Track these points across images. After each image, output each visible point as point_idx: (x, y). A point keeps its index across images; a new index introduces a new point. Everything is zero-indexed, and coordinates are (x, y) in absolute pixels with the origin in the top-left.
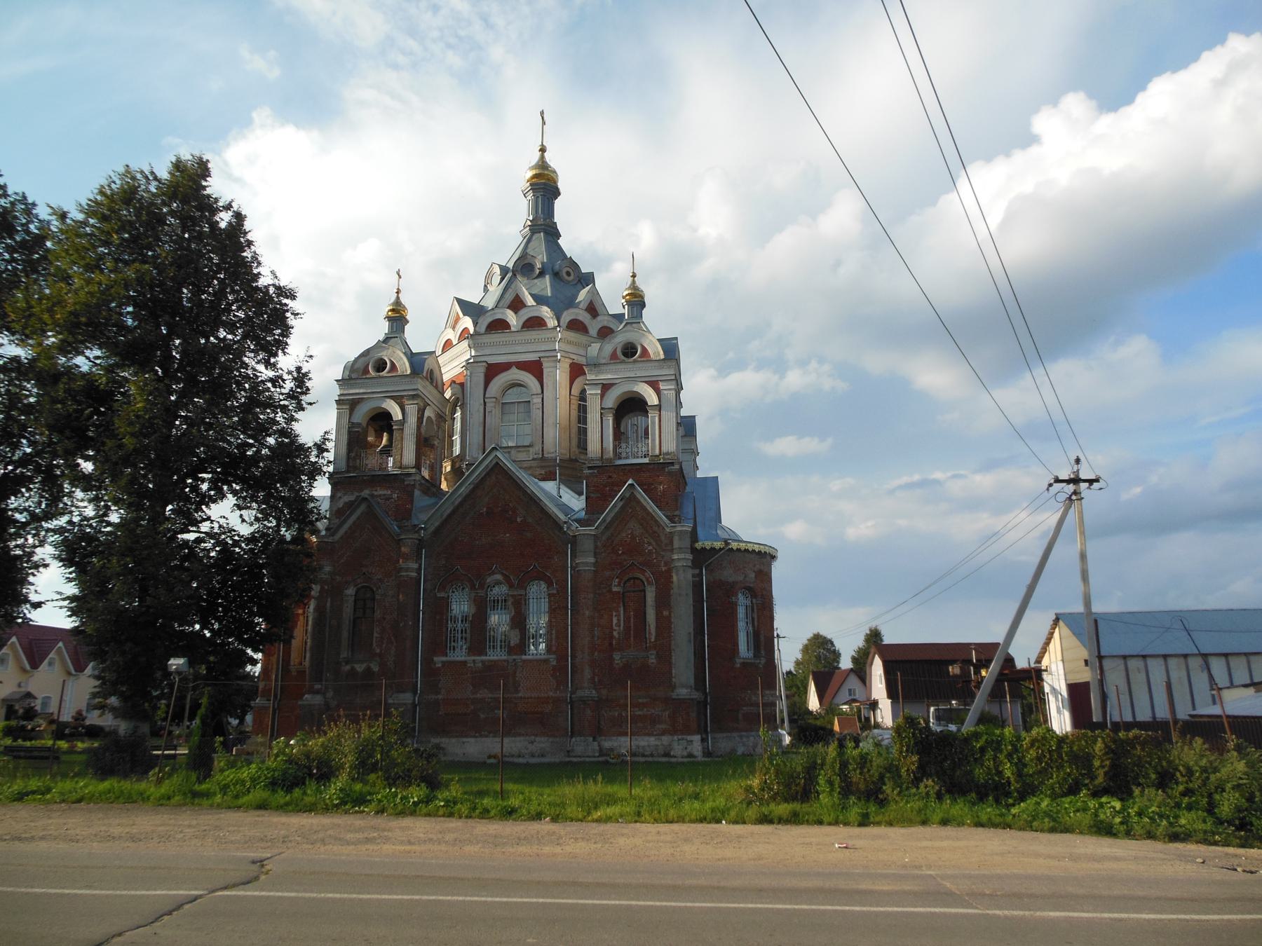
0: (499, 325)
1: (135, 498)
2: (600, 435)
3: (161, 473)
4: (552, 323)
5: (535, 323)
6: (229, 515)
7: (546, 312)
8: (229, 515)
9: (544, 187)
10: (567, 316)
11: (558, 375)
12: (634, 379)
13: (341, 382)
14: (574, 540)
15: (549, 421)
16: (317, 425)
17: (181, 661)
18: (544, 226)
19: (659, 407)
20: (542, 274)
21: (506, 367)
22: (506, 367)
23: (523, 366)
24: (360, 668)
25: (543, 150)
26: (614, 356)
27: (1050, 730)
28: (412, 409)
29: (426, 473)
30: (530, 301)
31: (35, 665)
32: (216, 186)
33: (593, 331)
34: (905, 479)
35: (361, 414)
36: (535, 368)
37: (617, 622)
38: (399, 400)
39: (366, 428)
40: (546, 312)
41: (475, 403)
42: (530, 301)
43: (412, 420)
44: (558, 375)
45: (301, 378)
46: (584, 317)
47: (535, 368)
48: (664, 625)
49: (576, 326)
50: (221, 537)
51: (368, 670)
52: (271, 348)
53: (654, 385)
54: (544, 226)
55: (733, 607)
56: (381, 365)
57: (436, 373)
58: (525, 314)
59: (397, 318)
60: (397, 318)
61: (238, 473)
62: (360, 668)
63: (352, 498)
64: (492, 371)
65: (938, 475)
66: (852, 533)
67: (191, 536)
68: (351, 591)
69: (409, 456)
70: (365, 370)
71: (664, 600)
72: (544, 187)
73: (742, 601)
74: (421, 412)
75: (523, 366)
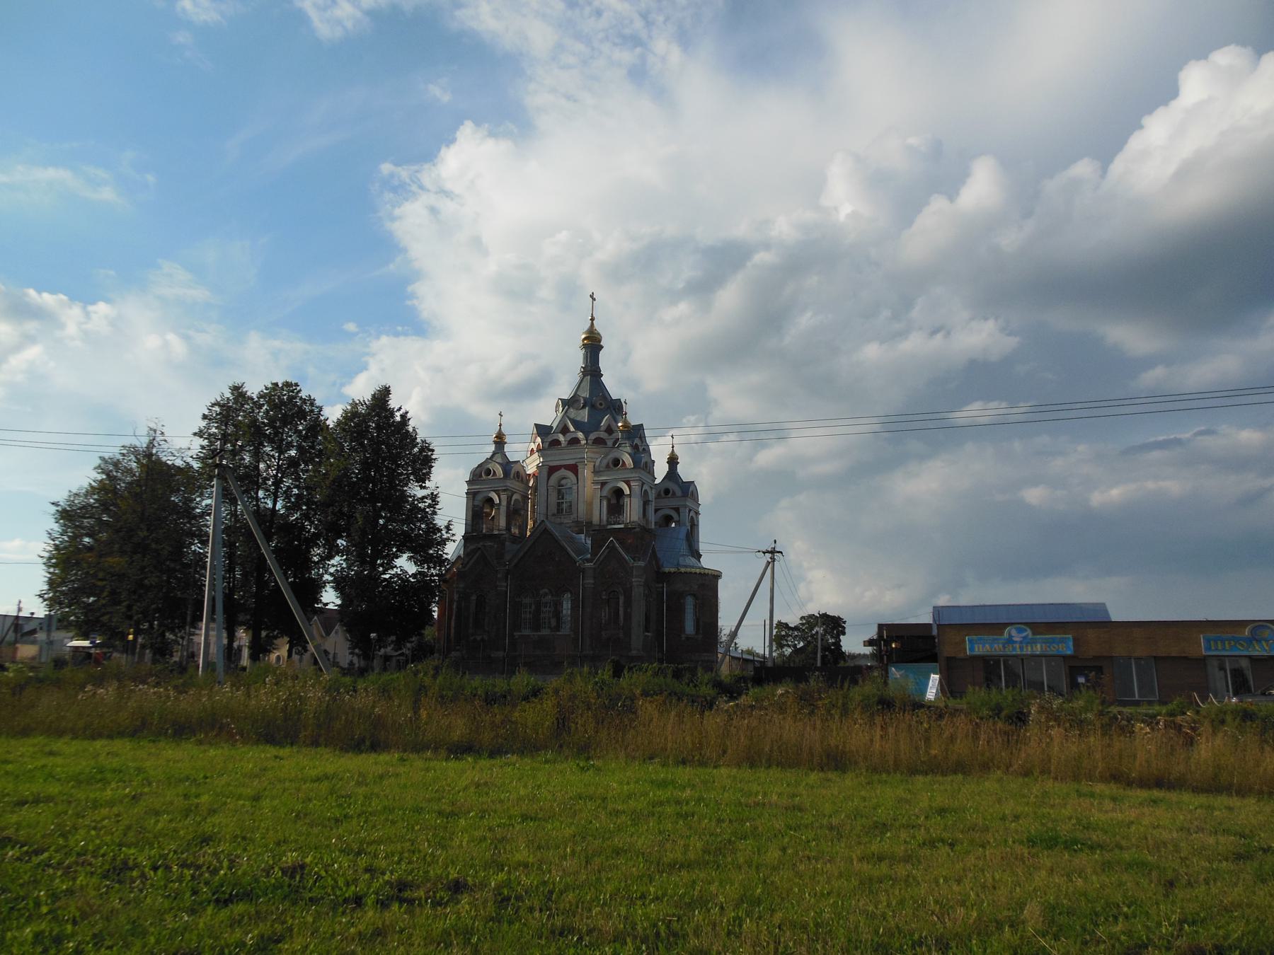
0: (556, 443)
1: (362, 559)
2: (599, 513)
3: (374, 548)
4: (583, 442)
5: (575, 441)
6: (405, 564)
7: (580, 435)
8: (405, 564)
9: (593, 344)
10: (593, 436)
12: (617, 480)
13: (469, 482)
14: (583, 571)
15: (581, 499)
16: (452, 513)
18: (592, 371)
19: (630, 496)
20: (584, 407)
21: (557, 468)
22: (557, 468)
23: (568, 467)
24: (479, 638)
25: (592, 319)
26: (608, 466)
28: (504, 497)
29: (515, 531)
30: (572, 429)
31: (328, 634)
32: (393, 403)
33: (610, 443)
34: (1196, 429)
35: (480, 497)
36: (574, 469)
38: (497, 492)
39: (478, 509)
40: (580, 435)
41: (542, 489)
42: (572, 429)
43: (504, 503)
45: (434, 497)
46: (603, 435)
48: (628, 617)
49: (599, 442)
50: (402, 578)
51: (483, 640)
52: (422, 478)
53: (628, 483)
54: (592, 371)
56: (488, 472)
57: (522, 472)
58: (569, 436)
59: (500, 441)
60: (500, 441)
62: (479, 638)
64: (552, 470)
65: (1185, 436)
66: (1097, 499)
67: (387, 576)
68: (474, 597)
69: (502, 522)
70: (479, 476)
72: (593, 344)
73: (689, 603)
74: (509, 499)
75: (568, 467)
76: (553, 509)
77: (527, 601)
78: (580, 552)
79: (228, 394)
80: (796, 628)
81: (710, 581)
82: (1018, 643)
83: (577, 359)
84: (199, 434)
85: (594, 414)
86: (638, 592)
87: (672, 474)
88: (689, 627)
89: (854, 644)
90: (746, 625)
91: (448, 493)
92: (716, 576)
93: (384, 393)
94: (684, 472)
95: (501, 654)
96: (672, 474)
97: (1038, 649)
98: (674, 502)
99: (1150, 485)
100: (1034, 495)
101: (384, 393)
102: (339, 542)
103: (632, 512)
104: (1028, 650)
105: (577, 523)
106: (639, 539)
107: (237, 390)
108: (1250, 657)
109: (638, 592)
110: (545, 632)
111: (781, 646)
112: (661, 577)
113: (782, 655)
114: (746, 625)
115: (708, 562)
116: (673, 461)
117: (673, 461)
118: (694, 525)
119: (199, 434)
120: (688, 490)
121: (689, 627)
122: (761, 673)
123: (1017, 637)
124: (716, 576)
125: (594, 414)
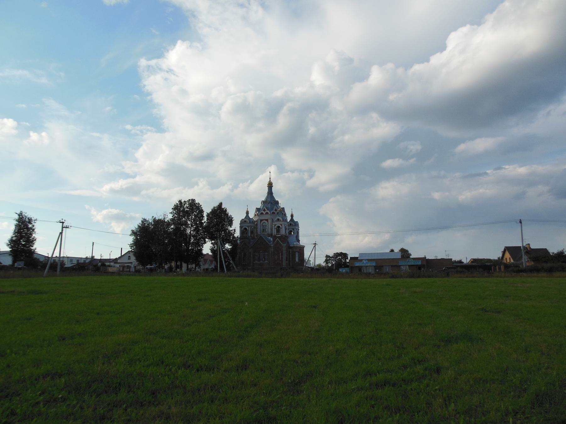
2: (274, 232)
7: (268, 211)
9: (270, 185)
11: (270, 221)
17: (229, 247)
18: (270, 193)
22: (263, 220)
27: (201, 250)
32: (223, 207)
37: (276, 257)
39: (243, 231)
44: (270, 221)
45: (235, 230)
47: (267, 220)
48: (282, 258)
54: (270, 193)
55: (295, 255)
61: (229, 242)
63: (417, 67)
64: (261, 220)
69: (249, 235)
70: (243, 222)
71: (282, 255)
72: (270, 185)
73: (297, 255)
76: (262, 230)
77: (256, 254)
78: (270, 241)
79: (177, 202)
80: (332, 257)
81: (302, 249)
82: (364, 263)
83: (266, 190)
84: (171, 213)
85: (271, 203)
86: (284, 252)
87: (292, 219)
88: (297, 260)
89: (411, 257)
90: (316, 257)
91: (236, 228)
92: (303, 247)
93: (221, 204)
94: (295, 219)
95: (250, 267)
96: (292, 219)
97: (369, 265)
98: (293, 227)
99: (481, 191)
100: (436, 195)
101: (221, 204)
102: (229, 247)
103: (283, 232)
104: (367, 265)
105: (268, 234)
106: (284, 239)
107: (180, 201)
108: (409, 266)
109: (284, 252)
110: (261, 262)
111: (327, 263)
112: (290, 248)
113: (328, 266)
114: (316, 257)
115: (302, 243)
116: (292, 216)
117: (292, 216)
118: (298, 233)
119: (171, 213)
120: (296, 224)
121: (297, 260)
122: (318, 270)
123: (365, 262)
124: (303, 247)
125: (271, 203)
